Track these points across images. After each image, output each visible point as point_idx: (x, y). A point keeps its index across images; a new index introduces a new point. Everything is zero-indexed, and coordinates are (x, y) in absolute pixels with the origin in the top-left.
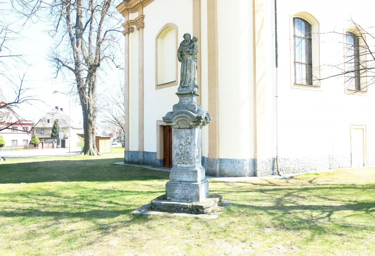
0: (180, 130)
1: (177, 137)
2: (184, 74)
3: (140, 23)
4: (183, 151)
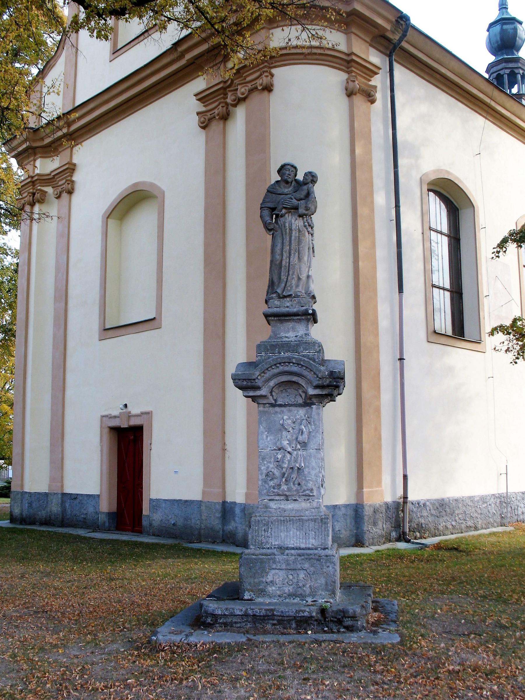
0: (277, 409)
1: (269, 430)
2: (284, 263)
3: (64, 181)
4: (286, 466)
